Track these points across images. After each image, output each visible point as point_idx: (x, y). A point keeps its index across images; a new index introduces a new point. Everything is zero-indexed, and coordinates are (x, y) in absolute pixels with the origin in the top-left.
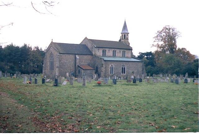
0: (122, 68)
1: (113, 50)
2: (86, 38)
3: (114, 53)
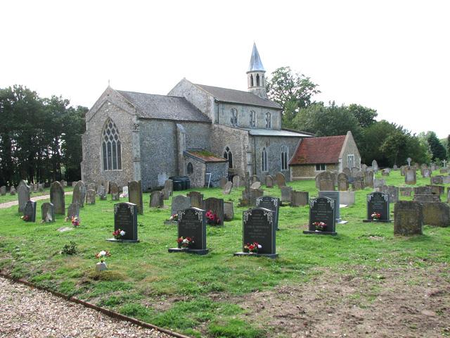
0: (283, 154)
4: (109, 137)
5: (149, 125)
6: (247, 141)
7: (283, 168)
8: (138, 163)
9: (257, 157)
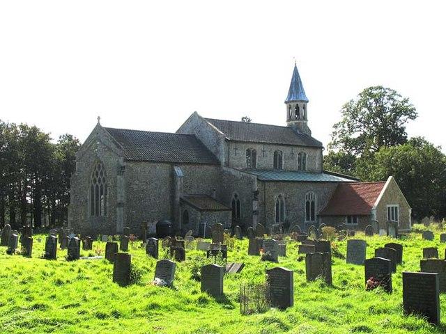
0: (308, 203)
2: (195, 113)
4: (97, 179)
7: (308, 219)
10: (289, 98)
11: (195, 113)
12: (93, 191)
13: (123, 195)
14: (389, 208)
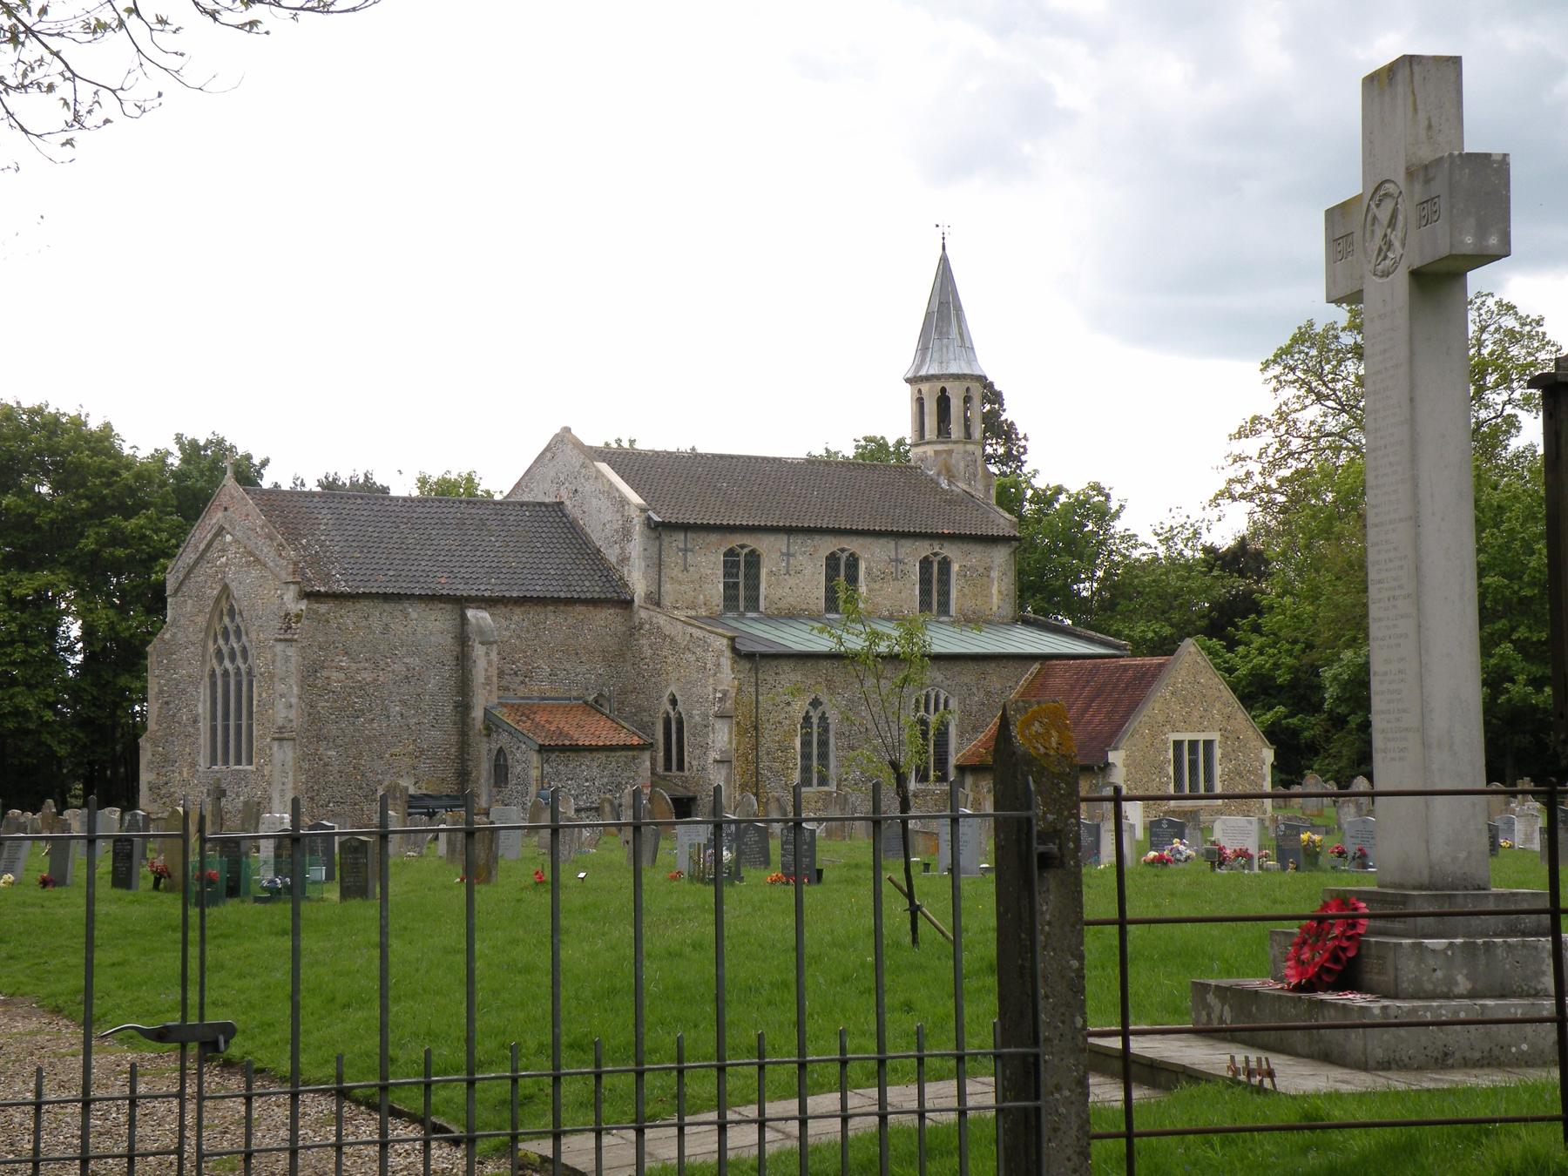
1: (829, 545)
2: (567, 430)
3: (842, 571)
5: (349, 616)
6: (727, 675)
8: (288, 746)
9: (769, 740)
10: (919, 367)
11: (567, 430)
12: (213, 685)
13: (294, 700)
14: (1178, 745)
